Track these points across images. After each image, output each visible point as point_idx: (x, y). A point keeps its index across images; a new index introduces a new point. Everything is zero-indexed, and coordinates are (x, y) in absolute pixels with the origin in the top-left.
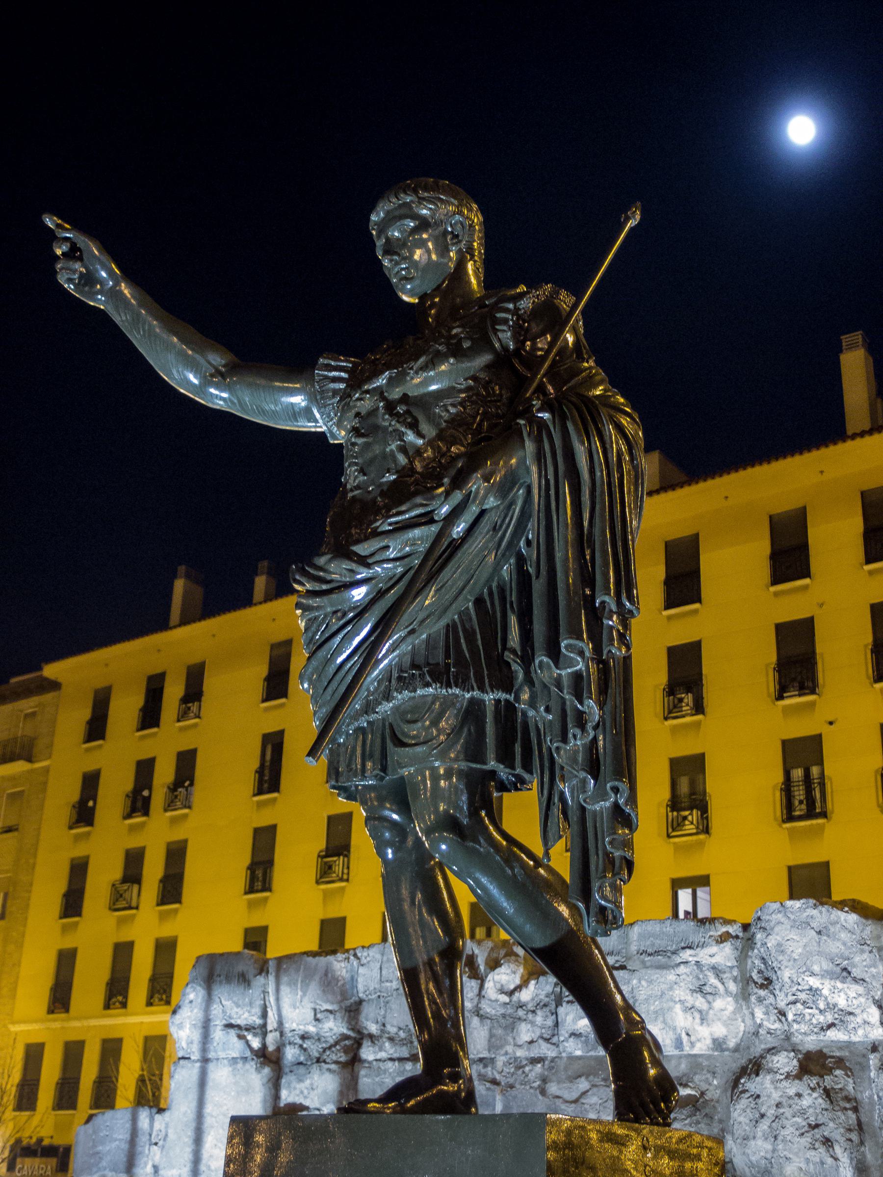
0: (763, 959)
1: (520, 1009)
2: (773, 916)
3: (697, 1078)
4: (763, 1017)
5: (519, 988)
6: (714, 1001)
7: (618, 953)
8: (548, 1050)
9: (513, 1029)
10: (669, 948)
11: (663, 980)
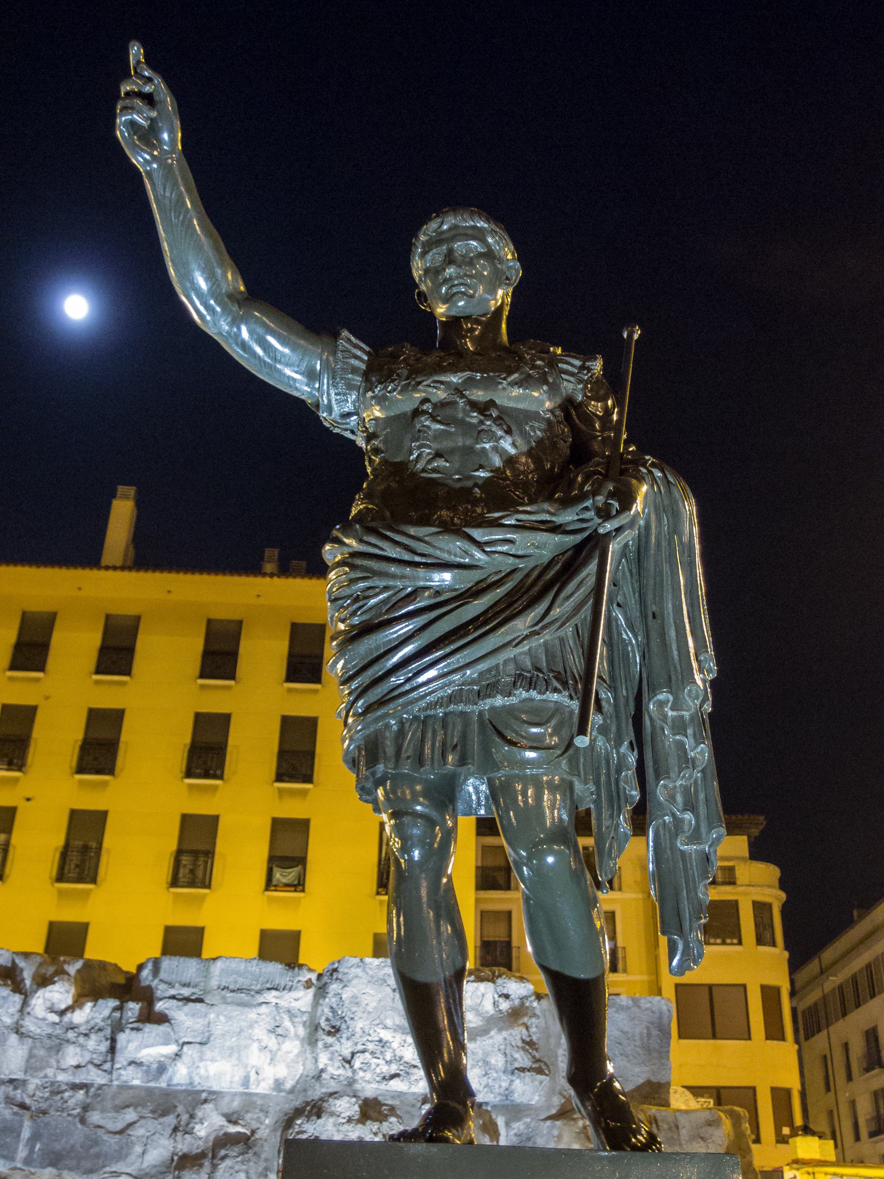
0: (332, 1008)
1: (70, 1031)
2: (352, 969)
3: (248, 1116)
4: (327, 1062)
5: (71, 1009)
6: (283, 1042)
7: (196, 986)
8: (98, 1076)
9: (58, 1051)
10: (253, 987)
11: (243, 1017)
